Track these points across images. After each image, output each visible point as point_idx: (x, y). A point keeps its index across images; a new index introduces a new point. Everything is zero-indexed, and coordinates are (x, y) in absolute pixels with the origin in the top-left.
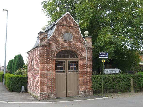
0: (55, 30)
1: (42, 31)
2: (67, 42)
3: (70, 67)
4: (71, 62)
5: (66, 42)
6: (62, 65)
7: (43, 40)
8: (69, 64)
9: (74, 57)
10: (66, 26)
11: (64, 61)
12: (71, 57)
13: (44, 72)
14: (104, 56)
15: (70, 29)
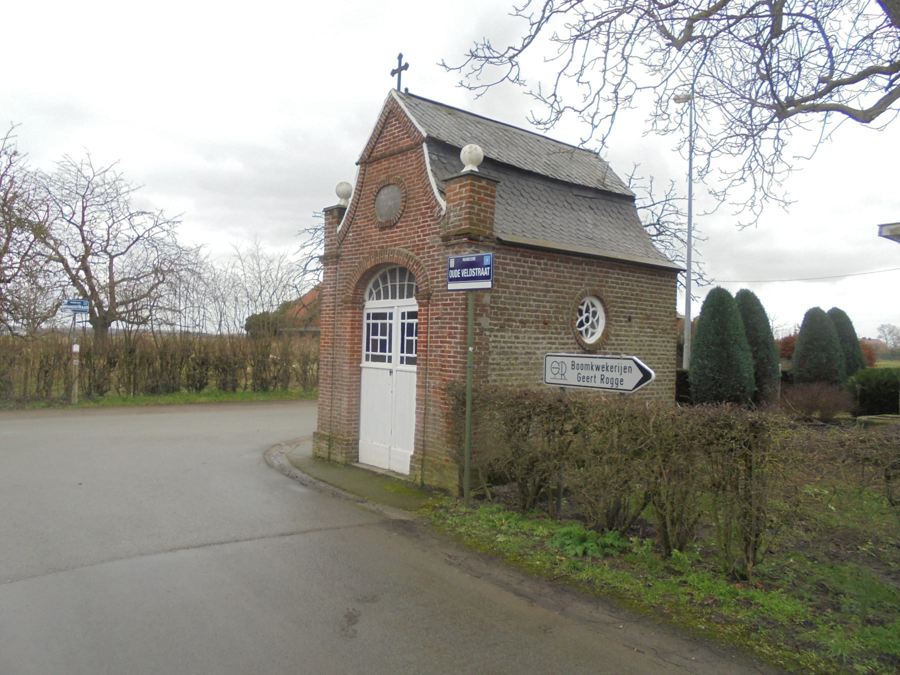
10: (402, 151)
14: (473, 272)
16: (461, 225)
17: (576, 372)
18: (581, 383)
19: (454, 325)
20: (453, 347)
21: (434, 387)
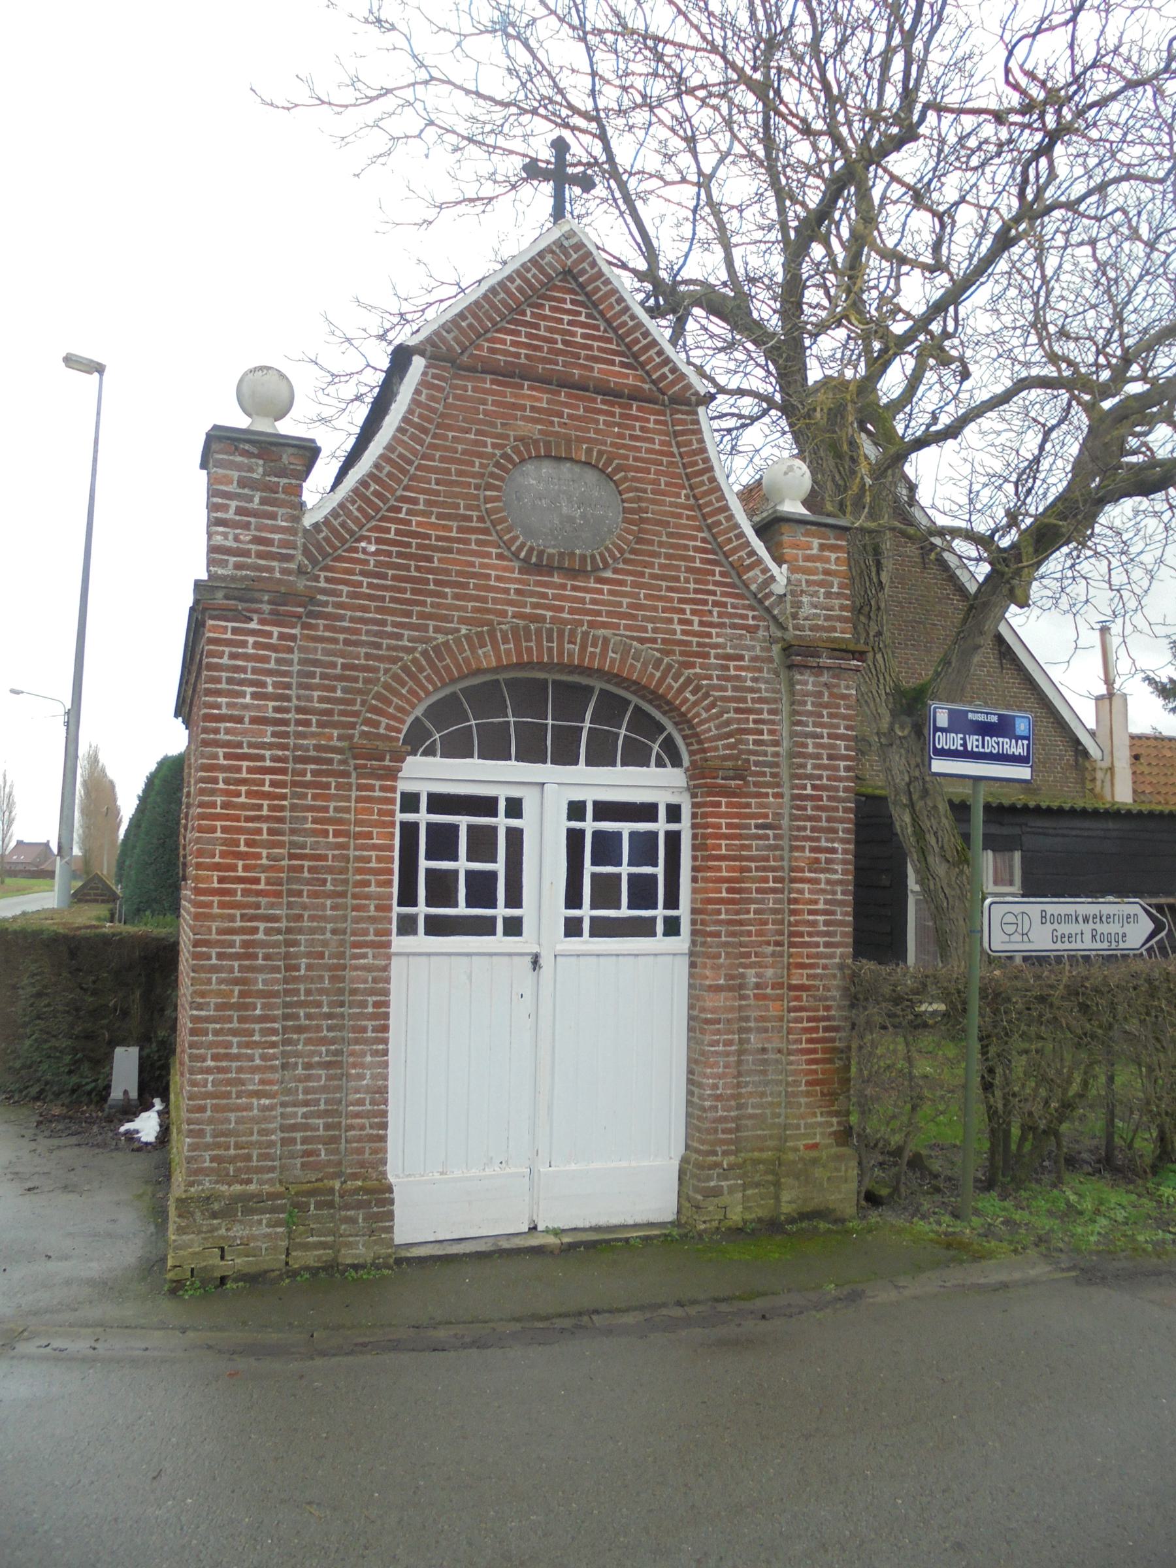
0: (405, 420)
1: (240, 421)
2: (549, 570)
3: (589, 869)
4: (605, 810)
5: (538, 566)
6: (482, 843)
7: (245, 536)
8: (575, 839)
9: (636, 756)
10: (544, 381)
11: (515, 793)
12: (600, 756)
13: (391, 636)
14: (992, 744)
15: (603, 425)
16: (834, 629)
17: (1049, 927)
18: (1059, 946)
19: (824, 844)
20: (823, 891)
21: (758, 986)
